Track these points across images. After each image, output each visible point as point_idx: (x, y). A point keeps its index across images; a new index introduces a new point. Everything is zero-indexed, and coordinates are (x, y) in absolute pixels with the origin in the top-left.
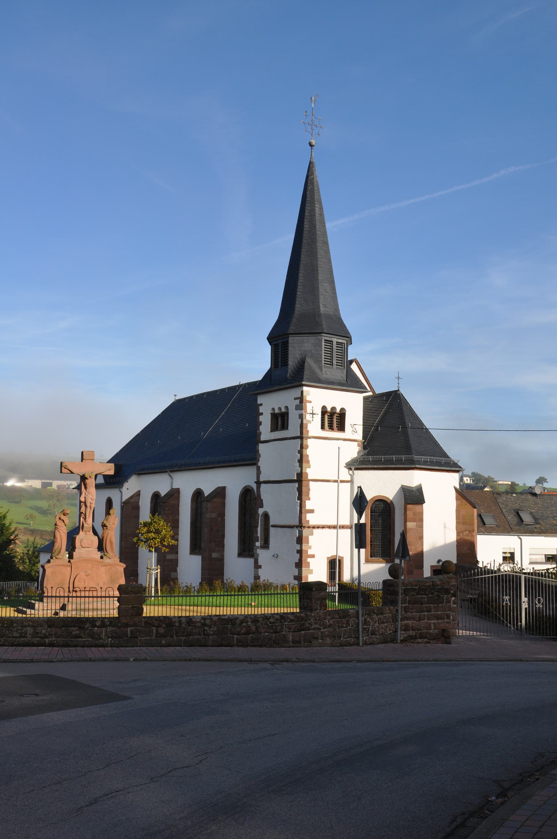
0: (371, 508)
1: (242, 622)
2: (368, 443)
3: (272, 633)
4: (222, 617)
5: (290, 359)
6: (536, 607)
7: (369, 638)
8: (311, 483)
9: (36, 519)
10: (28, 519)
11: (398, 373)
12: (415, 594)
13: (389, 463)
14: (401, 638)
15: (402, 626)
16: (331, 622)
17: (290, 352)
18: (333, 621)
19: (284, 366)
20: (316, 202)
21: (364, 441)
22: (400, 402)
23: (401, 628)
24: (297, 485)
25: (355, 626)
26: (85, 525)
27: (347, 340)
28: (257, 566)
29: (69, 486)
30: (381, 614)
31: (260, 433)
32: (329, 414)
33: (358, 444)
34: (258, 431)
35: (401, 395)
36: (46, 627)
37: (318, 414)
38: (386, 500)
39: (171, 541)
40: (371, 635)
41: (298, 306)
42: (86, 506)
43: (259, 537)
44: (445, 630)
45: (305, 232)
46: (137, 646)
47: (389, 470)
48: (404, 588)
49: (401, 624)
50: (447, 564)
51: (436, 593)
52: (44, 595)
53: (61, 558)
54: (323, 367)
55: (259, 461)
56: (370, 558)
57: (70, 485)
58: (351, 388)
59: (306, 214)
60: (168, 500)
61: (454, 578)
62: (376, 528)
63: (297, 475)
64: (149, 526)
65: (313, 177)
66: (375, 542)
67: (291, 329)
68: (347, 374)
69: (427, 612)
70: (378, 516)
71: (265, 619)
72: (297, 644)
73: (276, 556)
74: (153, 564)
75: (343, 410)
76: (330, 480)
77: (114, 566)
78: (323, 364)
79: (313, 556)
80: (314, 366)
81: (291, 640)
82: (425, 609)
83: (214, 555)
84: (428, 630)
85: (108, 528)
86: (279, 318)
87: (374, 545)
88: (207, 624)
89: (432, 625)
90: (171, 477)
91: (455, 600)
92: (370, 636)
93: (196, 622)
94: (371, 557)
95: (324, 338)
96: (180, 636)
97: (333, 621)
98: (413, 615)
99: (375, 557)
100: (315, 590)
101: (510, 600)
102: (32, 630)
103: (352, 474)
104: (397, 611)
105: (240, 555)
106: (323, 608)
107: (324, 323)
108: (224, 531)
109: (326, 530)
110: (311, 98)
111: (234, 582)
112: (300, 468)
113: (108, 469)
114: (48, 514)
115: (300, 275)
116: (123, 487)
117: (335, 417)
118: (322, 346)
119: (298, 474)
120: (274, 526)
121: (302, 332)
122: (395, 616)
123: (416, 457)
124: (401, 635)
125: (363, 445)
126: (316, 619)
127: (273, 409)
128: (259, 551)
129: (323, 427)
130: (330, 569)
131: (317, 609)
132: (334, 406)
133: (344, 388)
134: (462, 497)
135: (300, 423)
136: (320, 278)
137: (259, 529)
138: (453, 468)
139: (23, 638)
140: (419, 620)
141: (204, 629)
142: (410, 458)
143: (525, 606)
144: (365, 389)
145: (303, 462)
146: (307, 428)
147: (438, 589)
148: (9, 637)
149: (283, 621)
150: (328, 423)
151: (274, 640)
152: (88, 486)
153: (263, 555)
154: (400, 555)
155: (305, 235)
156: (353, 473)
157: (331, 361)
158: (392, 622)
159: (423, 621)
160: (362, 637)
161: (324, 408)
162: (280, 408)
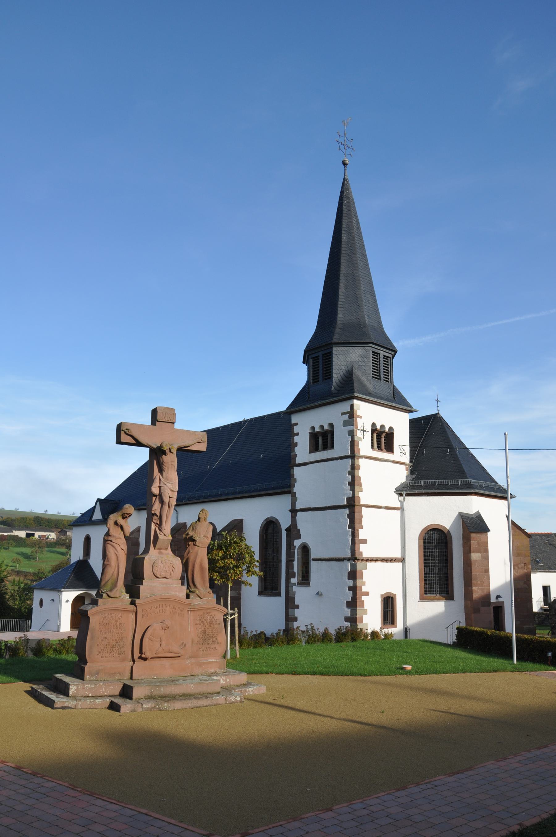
5: (334, 371)
8: (363, 509)
9: (21, 562)
10: (14, 562)
11: (437, 396)
17: (334, 363)
24: (347, 511)
26: (161, 537)
29: (48, 536)
31: (296, 456)
34: (292, 454)
41: (340, 316)
42: (162, 502)
43: (295, 573)
55: (294, 487)
57: (49, 535)
58: (400, 406)
59: (344, 226)
60: (175, 535)
62: (430, 561)
64: (227, 549)
77: (209, 611)
79: (367, 594)
99: (430, 594)
103: (403, 501)
109: (379, 564)
110: (343, 121)
112: (351, 492)
114: (31, 559)
117: (383, 436)
119: (348, 499)
120: (314, 560)
121: (348, 342)
123: (474, 482)
132: (383, 424)
133: (394, 404)
142: (463, 482)
145: (356, 485)
146: (358, 446)
152: (165, 468)
156: (404, 499)
161: (374, 425)
162: (322, 427)
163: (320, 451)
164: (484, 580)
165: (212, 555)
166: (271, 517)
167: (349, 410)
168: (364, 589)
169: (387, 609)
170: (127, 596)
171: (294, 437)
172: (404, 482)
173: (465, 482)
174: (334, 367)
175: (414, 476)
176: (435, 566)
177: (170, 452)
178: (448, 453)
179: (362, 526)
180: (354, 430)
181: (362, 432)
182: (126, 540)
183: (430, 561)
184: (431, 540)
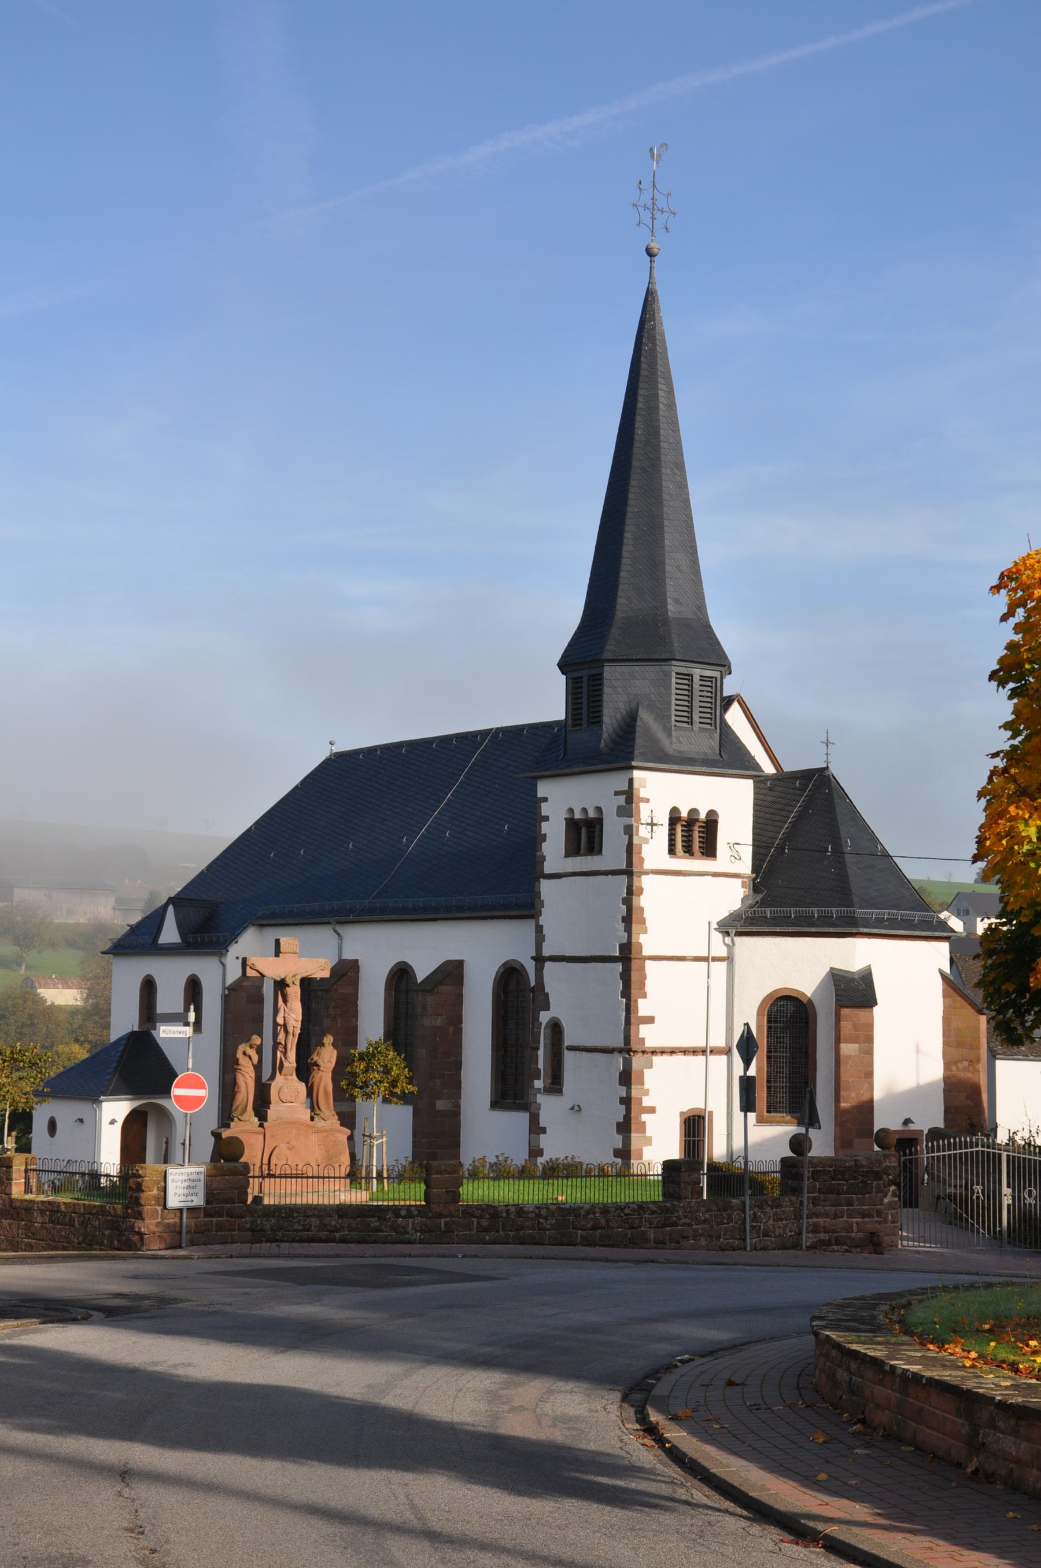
0: (768, 1012)
1: (588, 1213)
2: (762, 879)
3: (627, 1229)
4: (561, 1206)
5: (605, 711)
6: (1025, 1204)
7: (760, 1240)
8: (648, 963)
11: (827, 733)
12: (829, 1179)
13: (805, 922)
14: (808, 1243)
15: (809, 1225)
16: (707, 1216)
17: (605, 697)
18: (710, 1215)
19: (594, 723)
20: (659, 379)
21: (754, 875)
22: (830, 794)
23: (807, 1229)
24: (619, 967)
25: (739, 1223)
26: (286, 1064)
27: (721, 671)
28: (536, 1129)
30: (778, 1207)
31: (544, 858)
32: (684, 823)
33: (743, 883)
34: (538, 854)
35: (833, 780)
36: (336, 1218)
37: (662, 825)
38: (799, 997)
39: (407, 1087)
40: (763, 1237)
41: (621, 601)
42: (286, 1032)
43: (540, 1070)
44: (874, 1233)
45: (636, 444)
46: (454, 1243)
47: (806, 936)
48: (811, 1169)
49: (808, 1223)
50: (884, 1134)
51: (860, 1179)
52: (249, 1175)
53: (247, 1119)
54: (673, 728)
56: (766, 1114)
58: (729, 771)
59: (640, 405)
60: (335, 986)
61: (895, 1156)
62: (779, 1054)
63: (619, 948)
65: (655, 324)
66: (776, 1082)
67: (610, 650)
68: (720, 740)
69: (848, 1205)
70: (783, 1029)
71: (618, 1210)
72: (660, 1246)
73: (577, 1109)
74: (375, 1127)
75: (712, 813)
76: (685, 957)
77: (332, 1133)
78: (673, 723)
79: (652, 1110)
80: (655, 727)
81: (652, 1239)
82: (843, 1201)
83: (441, 1105)
84: (849, 1232)
85: (321, 1069)
86: (582, 622)
87: (776, 1087)
88: (542, 1215)
89: (855, 1225)
90: (338, 934)
91: (895, 1190)
92: (762, 1238)
93: (529, 1212)
94: (769, 1111)
95: (675, 669)
96: (508, 1231)
97: (710, 1215)
98: (826, 1210)
99: (776, 1112)
100: (685, 1171)
101: (983, 1191)
102: (318, 1222)
103: (731, 944)
104: (801, 1203)
105: (496, 1104)
106: (696, 1196)
107: (675, 638)
108: (460, 1054)
109: (679, 1058)
110: (651, 150)
111: (512, 1160)
113: (321, 968)
115: (626, 535)
116: (228, 953)
117: (696, 828)
118: (670, 686)
119: (621, 946)
120: (571, 1048)
121: (630, 657)
122: (798, 1210)
123: (860, 912)
124: (807, 1239)
125: (754, 883)
126: (686, 1212)
127: (571, 811)
128: (541, 1098)
129: (672, 851)
130: (685, 1137)
131: (686, 1197)
132: (693, 807)
133: (716, 770)
134: (955, 990)
135: (627, 842)
136: (667, 542)
137: (541, 1053)
138: (936, 931)
139: (307, 1231)
140: (835, 1218)
141: (538, 1221)
142: (847, 912)
143: (1007, 1201)
144: (758, 771)
146: (641, 853)
147: (863, 1172)
148: (288, 1231)
149: (641, 1212)
150: (683, 841)
151: (630, 1239)
152: (289, 999)
153: (549, 1107)
154: (806, 1121)
155: (638, 449)
157: (690, 715)
158: (794, 1219)
159: (841, 1219)
160: (750, 1238)
161: (674, 811)
162: (585, 810)
163: (582, 855)
164: (862, 1092)
165: (352, 1068)
166: (513, 960)
167: (627, 788)
168: (646, 1102)
169: (698, 1137)
170: (256, 1120)
171: (541, 823)
172: (735, 911)
173: (851, 913)
174: (605, 704)
175: (759, 897)
176: (786, 1064)
177: (294, 983)
178: (829, 854)
179: (645, 993)
180: (632, 825)
181: (649, 827)
182: (254, 1068)
183: (779, 1054)
184: (780, 1016)
